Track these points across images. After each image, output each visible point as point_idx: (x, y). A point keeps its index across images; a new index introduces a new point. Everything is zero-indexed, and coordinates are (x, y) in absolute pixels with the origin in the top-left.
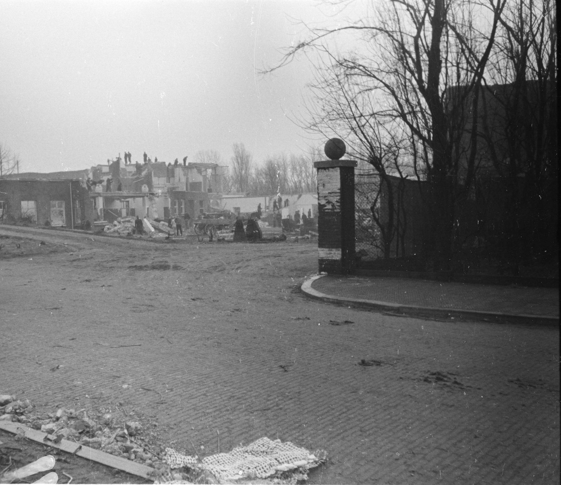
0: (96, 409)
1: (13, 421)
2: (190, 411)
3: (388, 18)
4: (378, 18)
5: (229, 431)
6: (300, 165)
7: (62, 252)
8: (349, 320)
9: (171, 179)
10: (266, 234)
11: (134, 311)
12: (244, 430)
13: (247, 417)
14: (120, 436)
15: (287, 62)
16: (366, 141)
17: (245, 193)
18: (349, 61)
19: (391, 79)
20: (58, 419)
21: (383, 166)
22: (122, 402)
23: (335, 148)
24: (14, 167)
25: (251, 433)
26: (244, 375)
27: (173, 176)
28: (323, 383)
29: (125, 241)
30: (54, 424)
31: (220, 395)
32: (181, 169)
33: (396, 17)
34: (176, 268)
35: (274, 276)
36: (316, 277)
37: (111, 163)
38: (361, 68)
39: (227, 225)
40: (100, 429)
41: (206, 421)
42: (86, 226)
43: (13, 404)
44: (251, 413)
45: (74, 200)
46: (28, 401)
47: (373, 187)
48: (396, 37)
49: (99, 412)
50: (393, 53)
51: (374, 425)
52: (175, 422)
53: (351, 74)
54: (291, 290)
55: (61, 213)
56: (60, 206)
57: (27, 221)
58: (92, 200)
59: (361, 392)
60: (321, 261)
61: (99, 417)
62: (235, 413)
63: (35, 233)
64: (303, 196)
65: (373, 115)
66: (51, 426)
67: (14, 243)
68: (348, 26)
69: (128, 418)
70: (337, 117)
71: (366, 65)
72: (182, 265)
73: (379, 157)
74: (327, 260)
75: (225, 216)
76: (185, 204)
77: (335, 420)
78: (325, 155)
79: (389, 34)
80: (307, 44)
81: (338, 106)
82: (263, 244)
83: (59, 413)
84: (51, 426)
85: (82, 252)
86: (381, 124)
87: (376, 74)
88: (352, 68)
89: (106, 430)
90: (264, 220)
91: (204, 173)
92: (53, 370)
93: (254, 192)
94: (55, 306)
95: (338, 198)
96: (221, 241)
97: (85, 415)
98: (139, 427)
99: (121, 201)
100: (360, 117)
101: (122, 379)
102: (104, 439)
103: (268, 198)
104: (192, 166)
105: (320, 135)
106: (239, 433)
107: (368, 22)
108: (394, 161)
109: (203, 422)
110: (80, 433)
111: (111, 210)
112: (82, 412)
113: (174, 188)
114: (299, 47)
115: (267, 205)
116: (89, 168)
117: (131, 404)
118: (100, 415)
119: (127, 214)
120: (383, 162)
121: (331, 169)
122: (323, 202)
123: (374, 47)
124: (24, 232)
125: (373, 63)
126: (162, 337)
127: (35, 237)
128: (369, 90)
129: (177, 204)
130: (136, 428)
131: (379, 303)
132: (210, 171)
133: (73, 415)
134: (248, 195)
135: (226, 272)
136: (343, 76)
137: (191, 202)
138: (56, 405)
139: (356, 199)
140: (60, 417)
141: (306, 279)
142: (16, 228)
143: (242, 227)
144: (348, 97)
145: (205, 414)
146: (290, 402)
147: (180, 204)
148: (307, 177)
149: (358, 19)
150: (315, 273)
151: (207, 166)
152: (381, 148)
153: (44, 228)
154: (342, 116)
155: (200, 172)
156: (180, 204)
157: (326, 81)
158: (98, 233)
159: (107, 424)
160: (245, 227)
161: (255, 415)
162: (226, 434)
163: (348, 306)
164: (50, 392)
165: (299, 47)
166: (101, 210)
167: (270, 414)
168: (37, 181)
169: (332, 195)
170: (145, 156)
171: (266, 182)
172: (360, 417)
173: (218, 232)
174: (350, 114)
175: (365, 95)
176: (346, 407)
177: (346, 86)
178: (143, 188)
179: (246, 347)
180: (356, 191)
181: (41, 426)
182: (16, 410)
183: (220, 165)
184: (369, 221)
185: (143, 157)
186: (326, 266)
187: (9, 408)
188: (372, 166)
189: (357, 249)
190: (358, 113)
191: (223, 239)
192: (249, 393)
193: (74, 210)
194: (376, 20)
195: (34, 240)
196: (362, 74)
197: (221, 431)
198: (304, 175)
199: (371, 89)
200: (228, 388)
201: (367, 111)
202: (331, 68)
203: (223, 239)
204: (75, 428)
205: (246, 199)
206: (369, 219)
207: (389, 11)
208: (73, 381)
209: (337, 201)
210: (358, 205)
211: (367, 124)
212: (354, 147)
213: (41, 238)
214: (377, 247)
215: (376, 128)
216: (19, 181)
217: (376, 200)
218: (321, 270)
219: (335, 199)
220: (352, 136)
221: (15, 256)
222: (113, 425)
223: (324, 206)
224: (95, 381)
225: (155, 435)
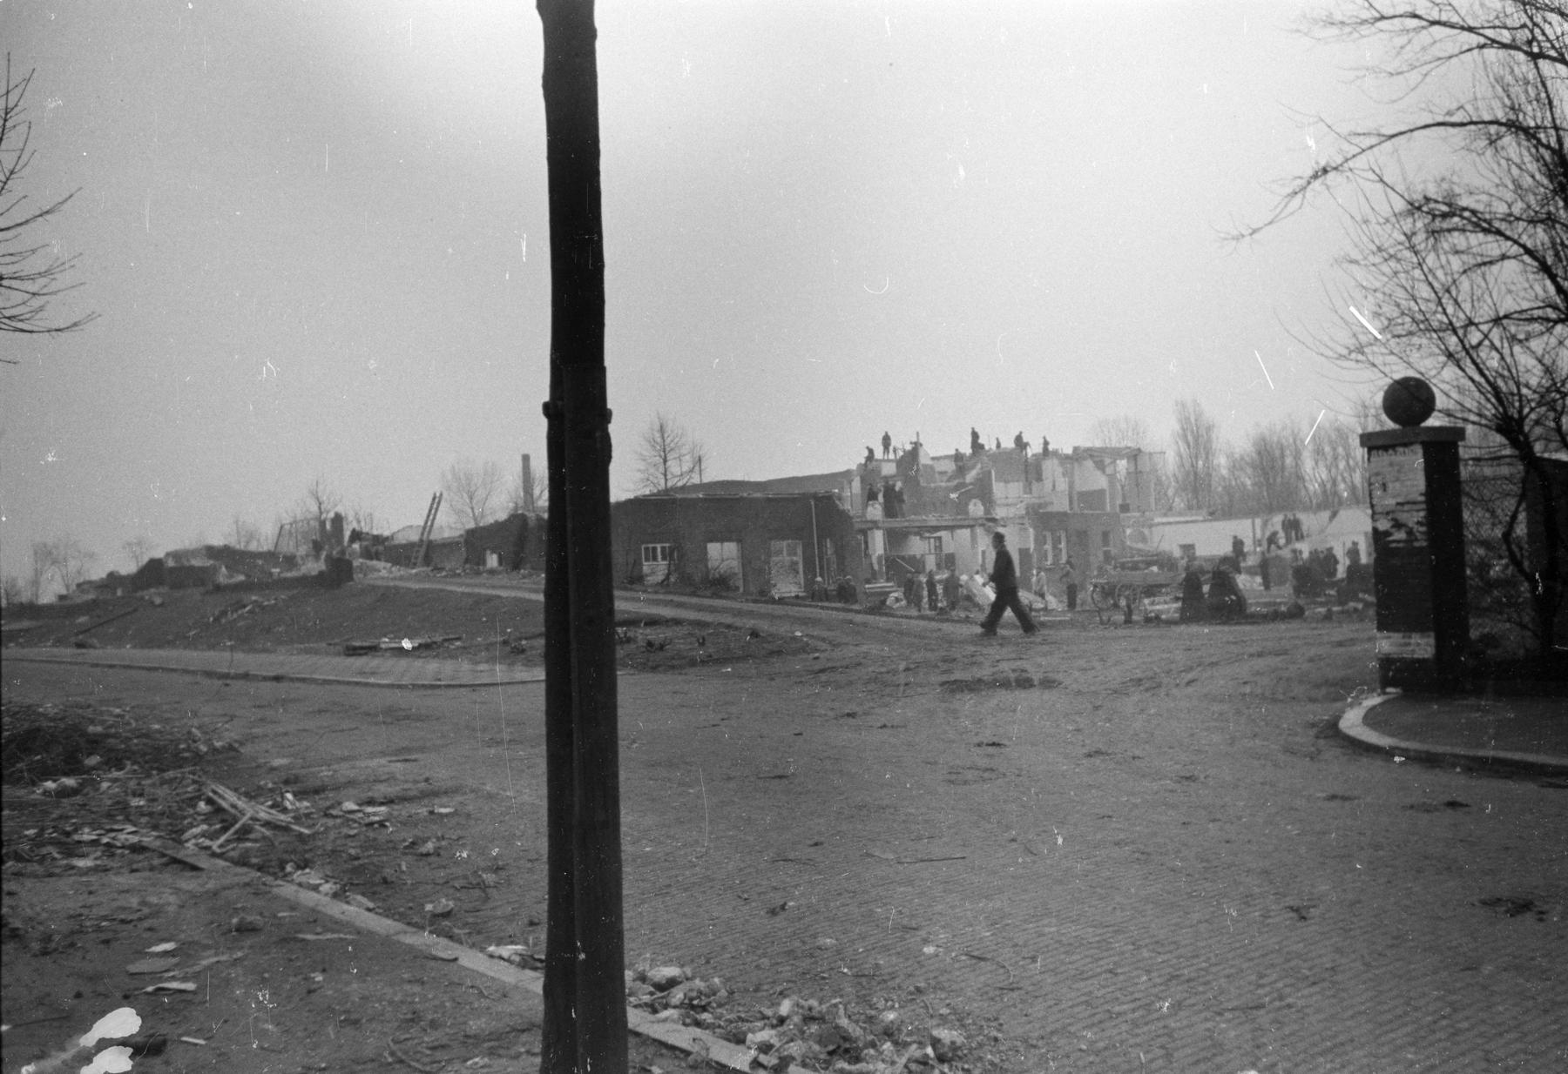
0: (864, 1000)
1: (684, 1024)
2: (1076, 1010)
3: (1523, 99)
4: (1500, 99)
5: (1168, 1056)
6: (1331, 442)
7: (795, 653)
8: (1459, 799)
9: (1035, 486)
10: (1258, 604)
11: (951, 782)
12: (1203, 1054)
13: (1209, 1025)
14: (917, 1062)
15: (1287, 211)
16: (1482, 380)
17: (1204, 512)
18: (1436, 202)
19: (1539, 237)
20: (782, 1021)
21: (1526, 436)
22: (922, 985)
23: (1409, 400)
24: (692, 471)
25: (1219, 1059)
26: (1202, 927)
27: (1039, 479)
28: (1392, 946)
29: (934, 625)
30: (773, 1032)
31: (1148, 972)
32: (1056, 461)
33: (1543, 95)
34: (1048, 684)
35: (1274, 701)
36: (1374, 700)
37: (901, 453)
38: (1466, 214)
39: (1166, 586)
40: (873, 1045)
41: (1115, 1032)
42: (846, 594)
43: (685, 986)
44: (1220, 1014)
45: (821, 539)
46: (716, 980)
47: (1509, 487)
48: (1544, 141)
49: (871, 1007)
50: (1538, 176)
51: (1519, 1046)
52: (1042, 1032)
53: (1442, 231)
54: (1315, 730)
55: (793, 567)
56: (792, 552)
57: (720, 585)
58: (860, 537)
59: (1488, 969)
60: (1386, 662)
61: (870, 1020)
62: (1182, 1014)
63: (739, 613)
64: (1343, 514)
65: (1497, 321)
66: (766, 1035)
67: (691, 635)
68: (1430, 121)
69: (934, 1022)
70: (1414, 328)
71: (1480, 207)
72: (1060, 677)
73: (1516, 416)
74: (1402, 660)
75: (1161, 567)
76: (1068, 542)
77: (1423, 1033)
78: (1384, 417)
79: (1530, 133)
80: (1336, 169)
81: (1412, 303)
82: (1248, 628)
83: (785, 1008)
84: (766, 1035)
85: (837, 654)
86: (1520, 341)
87: (1503, 226)
88: (1444, 216)
89: (887, 1046)
90: (1251, 572)
91: (1109, 470)
92: (773, 912)
93: (1226, 511)
94: (779, 772)
95: (1422, 514)
96: (1153, 621)
97: (841, 1011)
98: (960, 1040)
99: (922, 538)
100: (1465, 327)
101: (923, 933)
102: (881, 1066)
103: (1258, 521)
104: (1079, 455)
105: (1370, 374)
106: (1191, 1060)
107: (1477, 109)
108: (1552, 424)
109: (1107, 1033)
110: (831, 1053)
111: (903, 558)
112: (835, 1005)
113: (1040, 506)
114: (1315, 176)
115: (1259, 535)
116: (854, 467)
117: (943, 989)
118: (873, 1013)
119: (938, 566)
120: (1526, 429)
121: (1401, 449)
122: (1384, 525)
123: (1495, 167)
124: (713, 610)
125: (1495, 203)
126: (1014, 840)
127: (738, 622)
128: (1484, 264)
129: (1049, 541)
130: (953, 1043)
131: (1531, 758)
132: (1122, 464)
133: (814, 1013)
134: (1213, 515)
135: (1162, 692)
136: (1421, 236)
137: (1082, 535)
138: (779, 989)
139: (1466, 515)
140: (788, 1017)
141: (1351, 705)
142: (694, 600)
143: (1199, 587)
144: (1436, 285)
145: (1111, 1016)
146: (1312, 990)
147: (1056, 542)
148: (1351, 469)
149: (1455, 105)
150: (1373, 690)
151: (1116, 453)
152: (1520, 395)
153: (755, 601)
154: (1423, 325)
155: (1100, 466)
156: (1056, 542)
157: (1380, 249)
158: (871, 611)
159: (889, 1033)
160: (1206, 588)
161: (1229, 1021)
162: (1160, 1062)
163: (1454, 766)
164: (765, 962)
165: (1315, 176)
166: (880, 558)
167: (1263, 1018)
168: (742, 498)
169: (1406, 508)
170: (975, 436)
171: (1254, 484)
172: (1483, 1028)
173: (1146, 601)
174: (1441, 322)
175: (1476, 276)
176: (1451, 1004)
177: (1431, 260)
178: (971, 507)
179: (1207, 861)
180: (1465, 500)
181: (745, 1034)
182: (691, 999)
183: (1146, 448)
184: (1506, 567)
185: (969, 439)
186: (1395, 673)
187: (678, 995)
188: (1499, 439)
189: (1474, 634)
190: (1462, 316)
191: (1157, 618)
192: (1214, 969)
193: (821, 559)
194: (1496, 104)
195: (737, 628)
196: (1470, 227)
197: (1150, 1056)
198: (1342, 465)
199: (1491, 263)
200: (1165, 957)
201: (1484, 313)
202: (1393, 220)
203: (1157, 618)
204: (819, 1042)
205: (1208, 524)
206: (1504, 562)
207: (1527, 83)
208: (815, 936)
209: (1418, 523)
210: (1472, 529)
211: (1487, 342)
212: (1453, 393)
213: (750, 623)
214: (1523, 627)
215: (1506, 351)
216: (705, 500)
217: (1514, 517)
218: (1386, 683)
219: (1414, 518)
220: (1450, 372)
221: (693, 663)
222: (903, 1037)
223: (1387, 533)
224: (863, 937)
225: (997, 1061)
